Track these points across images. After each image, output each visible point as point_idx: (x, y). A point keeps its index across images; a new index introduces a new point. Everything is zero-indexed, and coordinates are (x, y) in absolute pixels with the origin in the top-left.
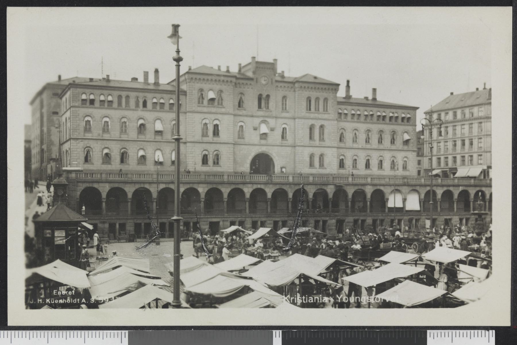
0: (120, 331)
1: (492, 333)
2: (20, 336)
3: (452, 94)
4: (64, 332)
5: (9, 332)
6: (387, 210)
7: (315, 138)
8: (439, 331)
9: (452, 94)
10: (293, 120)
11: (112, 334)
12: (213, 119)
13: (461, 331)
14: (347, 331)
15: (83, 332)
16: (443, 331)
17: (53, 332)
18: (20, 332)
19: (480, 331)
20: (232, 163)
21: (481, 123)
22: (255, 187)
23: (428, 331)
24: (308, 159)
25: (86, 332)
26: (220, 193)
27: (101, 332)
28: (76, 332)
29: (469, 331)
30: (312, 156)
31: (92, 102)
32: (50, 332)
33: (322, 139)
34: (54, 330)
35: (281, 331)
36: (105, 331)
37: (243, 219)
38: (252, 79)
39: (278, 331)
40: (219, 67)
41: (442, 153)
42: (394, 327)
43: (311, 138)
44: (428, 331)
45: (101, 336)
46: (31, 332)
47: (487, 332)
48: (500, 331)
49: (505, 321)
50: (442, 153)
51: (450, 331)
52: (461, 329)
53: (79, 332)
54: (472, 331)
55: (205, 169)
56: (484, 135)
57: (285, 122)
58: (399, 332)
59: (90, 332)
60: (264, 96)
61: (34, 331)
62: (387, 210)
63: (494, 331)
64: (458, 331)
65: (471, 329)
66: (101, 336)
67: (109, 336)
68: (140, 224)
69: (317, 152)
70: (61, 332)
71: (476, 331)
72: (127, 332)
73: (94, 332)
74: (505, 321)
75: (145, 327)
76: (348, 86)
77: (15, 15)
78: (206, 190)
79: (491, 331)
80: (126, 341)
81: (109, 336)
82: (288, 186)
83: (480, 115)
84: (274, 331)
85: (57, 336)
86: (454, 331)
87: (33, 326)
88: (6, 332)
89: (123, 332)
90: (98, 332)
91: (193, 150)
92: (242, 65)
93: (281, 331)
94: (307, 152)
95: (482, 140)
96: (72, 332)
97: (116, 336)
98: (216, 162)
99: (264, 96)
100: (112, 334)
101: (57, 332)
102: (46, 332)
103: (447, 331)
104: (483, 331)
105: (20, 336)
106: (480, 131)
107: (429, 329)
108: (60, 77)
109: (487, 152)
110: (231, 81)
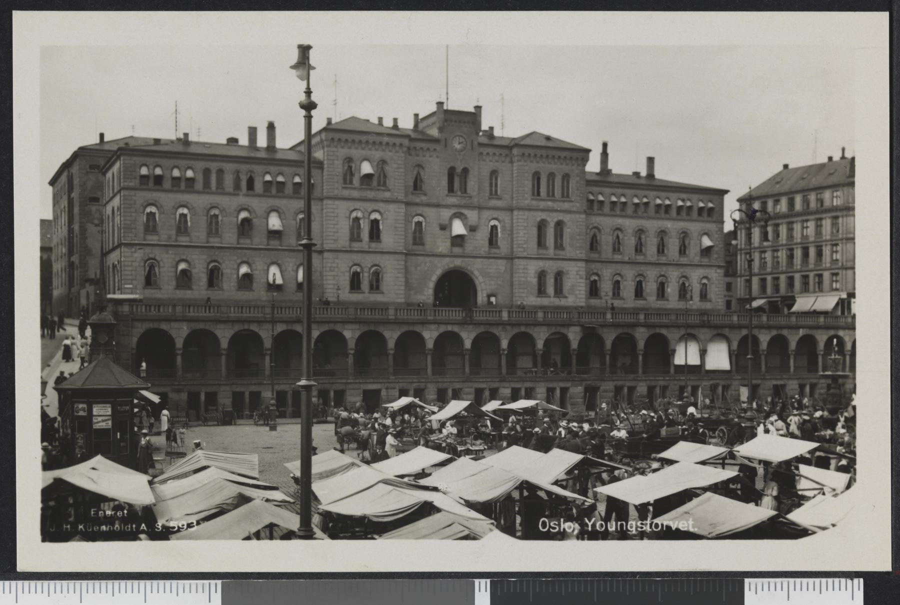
0: (206, 582)
1: (859, 583)
3: (786, 166)
4: (110, 582)
5: (20, 583)
6: (672, 370)
8: (766, 580)
9: (786, 166)
10: (508, 213)
11: (193, 587)
12: (370, 210)
13: (805, 580)
14: (605, 581)
15: (142, 582)
16: (772, 580)
17: (91, 583)
19: (837, 580)
20: (403, 288)
23: (747, 580)
24: (535, 281)
25: (148, 582)
27: (174, 582)
28: (129, 582)
29: (817, 580)
30: (542, 275)
31: (159, 180)
32: (84, 583)
33: (559, 246)
35: (488, 581)
37: (422, 385)
39: (483, 581)
40: (380, 119)
43: (541, 243)
44: (747, 580)
46: (52, 583)
47: (849, 581)
48: (871, 580)
49: (883, 562)
51: (785, 580)
52: (804, 577)
53: (136, 582)
54: (824, 580)
55: (356, 297)
58: (701, 581)
59: (155, 582)
60: (459, 170)
61: (64, 582)
62: (672, 370)
63: (862, 580)
64: (798, 580)
67: (187, 589)
68: (243, 393)
69: (551, 267)
71: (830, 580)
72: (219, 582)
74: (883, 562)
78: (357, 334)
79: (856, 581)
80: (217, 598)
81: (187, 589)
82: (500, 328)
83: (835, 204)
84: (477, 581)
85: (97, 590)
86: (792, 580)
88: (13, 583)
89: (213, 582)
90: (168, 582)
91: (334, 265)
92: (420, 117)
93: (488, 581)
94: (533, 267)
97: (200, 589)
98: (376, 285)
99: (459, 170)
100: (193, 587)
101: (97, 583)
102: (78, 583)
103: (779, 580)
104: (843, 580)
107: (748, 577)
108: (102, 136)
110: (401, 145)
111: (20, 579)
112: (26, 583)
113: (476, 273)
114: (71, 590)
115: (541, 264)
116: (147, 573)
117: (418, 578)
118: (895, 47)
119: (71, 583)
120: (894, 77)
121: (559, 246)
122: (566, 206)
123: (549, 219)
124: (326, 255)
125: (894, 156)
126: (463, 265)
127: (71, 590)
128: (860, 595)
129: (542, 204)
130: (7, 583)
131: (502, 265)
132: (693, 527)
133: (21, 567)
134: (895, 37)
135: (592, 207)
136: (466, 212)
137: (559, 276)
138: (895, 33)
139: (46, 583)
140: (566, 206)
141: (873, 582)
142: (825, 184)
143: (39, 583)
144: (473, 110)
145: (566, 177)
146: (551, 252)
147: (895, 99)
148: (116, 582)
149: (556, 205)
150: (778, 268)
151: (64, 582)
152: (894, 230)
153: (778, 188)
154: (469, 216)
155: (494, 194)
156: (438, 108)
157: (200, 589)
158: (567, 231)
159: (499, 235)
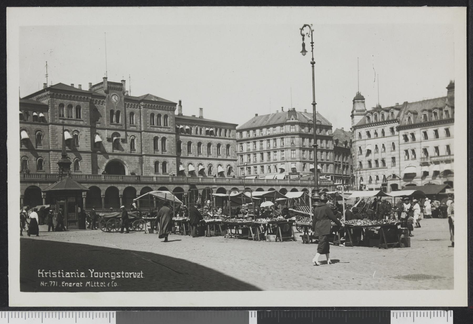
0: (108, 312)
1: (451, 313)
2: (17, 316)
3: (257, 115)
4: (57, 312)
5: (10, 312)
7: (159, 148)
8: (402, 311)
9: (257, 115)
10: (140, 134)
11: (101, 315)
12: (73, 130)
13: (422, 311)
15: (74, 312)
16: (405, 311)
17: (47, 312)
18: (17, 312)
19: (439, 311)
20: (91, 169)
21: (241, 144)
22: (127, 186)
23: (392, 311)
24: (153, 166)
25: (78, 312)
26: (99, 191)
27: (91, 312)
28: (68, 312)
29: (429, 311)
30: (156, 163)
32: (44, 312)
33: (164, 150)
34: (48, 310)
35: (256, 311)
36: (95, 312)
38: (104, 97)
39: (253, 312)
41: (252, 163)
42: (360, 307)
43: (156, 147)
44: (392, 311)
45: (91, 316)
46: (27, 312)
47: (445, 312)
48: (457, 311)
49: (463, 302)
50: (252, 163)
51: (412, 311)
52: (422, 310)
53: (71, 312)
56: (285, 148)
57: (133, 134)
59: (81, 312)
60: (115, 112)
61: (33, 312)
63: (452, 311)
64: (419, 311)
65: (431, 310)
66: (91, 316)
67: (98, 316)
69: (161, 160)
70: (54, 312)
71: (436, 311)
72: (115, 312)
73: (84, 312)
74: (463, 302)
75: (132, 307)
76: (180, 105)
77: (15, 16)
79: (449, 312)
80: (114, 320)
81: (98, 316)
83: (292, 131)
84: (250, 312)
85: (67, 316)
86: (415, 311)
87: (69, 307)
88: (7, 312)
89: (112, 312)
90: (88, 312)
91: (56, 157)
92: (93, 85)
93: (256, 311)
94: (153, 159)
95: (284, 152)
96: (64, 312)
97: (105, 316)
99: (115, 112)
100: (101, 315)
101: (51, 312)
102: (41, 312)
103: (409, 311)
104: (442, 311)
105: (17, 316)
106: (282, 145)
107: (392, 310)
109: (288, 162)
111: (10, 310)
112: (14, 312)
113: (125, 162)
114: (37, 316)
115: (156, 158)
116: (77, 307)
117: (220, 310)
118: (470, 31)
119: (88, 312)
120: (469, 46)
121: (164, 150)
122: (166, 130)
123: (159, 136)
124: (51, 152)
125: (470, 88)
126: (119, 158)
127: (37, 316)
128: (451, 319)
129: (156, 129)
130: (3, 312)
131: (137, 159)
132: (443, 280)
133: (11, 304)
134: (470, 25)
135: (178, 132)
136: (119, 132)
137: (164, 164)
138: (470, 23)
139: (24, 312)
140: (166, 130)
141: (458, 312)
142: (277, 123)
143: (20, 312)
144: (121, 82)
145: (166, 116)
146: (160, 153)
147: (470, 58)
148: (61, 312)
149: (162, 130)
150: (256, 162)
151: (34, 312)
152: (469, 127)
153: (254, 125)
154: (121, 134)
155: (132, 124)
156: (104, 80)
157: (105, 316)
158: (167, 142)
159: (135, 143)
